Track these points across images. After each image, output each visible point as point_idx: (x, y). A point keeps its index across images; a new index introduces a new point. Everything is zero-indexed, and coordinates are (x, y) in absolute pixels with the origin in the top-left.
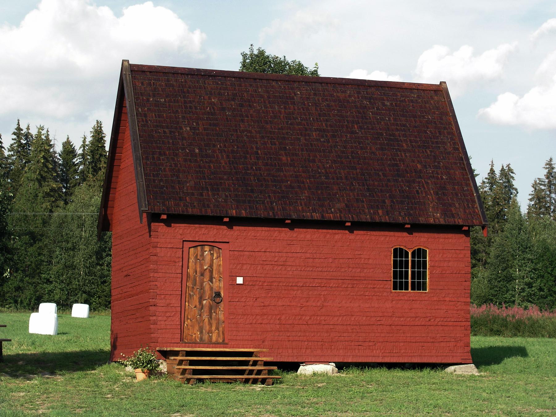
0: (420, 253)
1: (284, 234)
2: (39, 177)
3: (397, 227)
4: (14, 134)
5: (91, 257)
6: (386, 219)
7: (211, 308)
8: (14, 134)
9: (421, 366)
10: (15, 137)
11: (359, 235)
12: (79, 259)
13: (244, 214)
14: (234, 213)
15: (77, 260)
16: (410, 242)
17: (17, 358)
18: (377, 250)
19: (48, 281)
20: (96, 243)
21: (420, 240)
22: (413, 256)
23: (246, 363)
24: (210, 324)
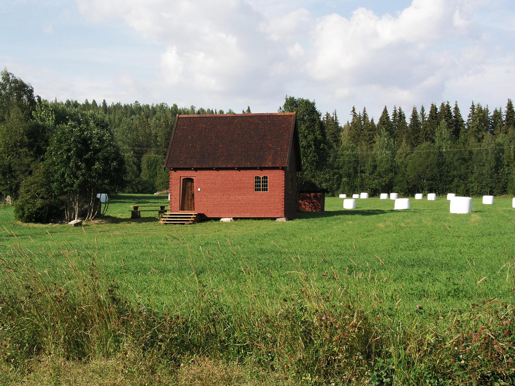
0: (265, 178)
1: (214, 173)
2: (477, 130)
3: (255, 169)
4: (471, 108)
5: (492, 169)
6: (250, 166)
7: (191, 199)
8: (471, 108)
9: (249, 218)
10: (471, 110)
11: (242, 172)
12: (485, 170)
13: (198, 167)
14: (195, 166)
15: (484, 171)
16: (261, 174)
17: (144, 218)
18: (249, 177)
19: (472, 182)
20: (494, 163)
21: (265, 173)
22: (262, 179)
23: (190, 218)
24: (191, 205)
